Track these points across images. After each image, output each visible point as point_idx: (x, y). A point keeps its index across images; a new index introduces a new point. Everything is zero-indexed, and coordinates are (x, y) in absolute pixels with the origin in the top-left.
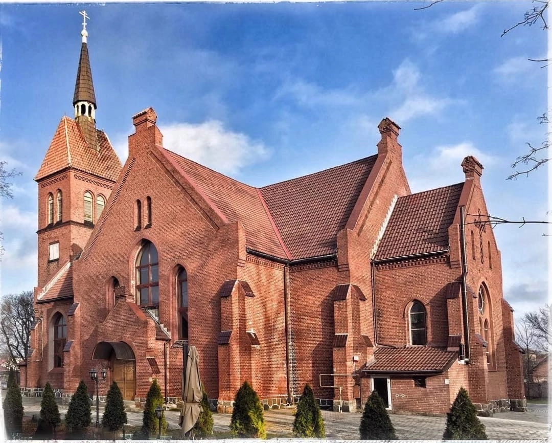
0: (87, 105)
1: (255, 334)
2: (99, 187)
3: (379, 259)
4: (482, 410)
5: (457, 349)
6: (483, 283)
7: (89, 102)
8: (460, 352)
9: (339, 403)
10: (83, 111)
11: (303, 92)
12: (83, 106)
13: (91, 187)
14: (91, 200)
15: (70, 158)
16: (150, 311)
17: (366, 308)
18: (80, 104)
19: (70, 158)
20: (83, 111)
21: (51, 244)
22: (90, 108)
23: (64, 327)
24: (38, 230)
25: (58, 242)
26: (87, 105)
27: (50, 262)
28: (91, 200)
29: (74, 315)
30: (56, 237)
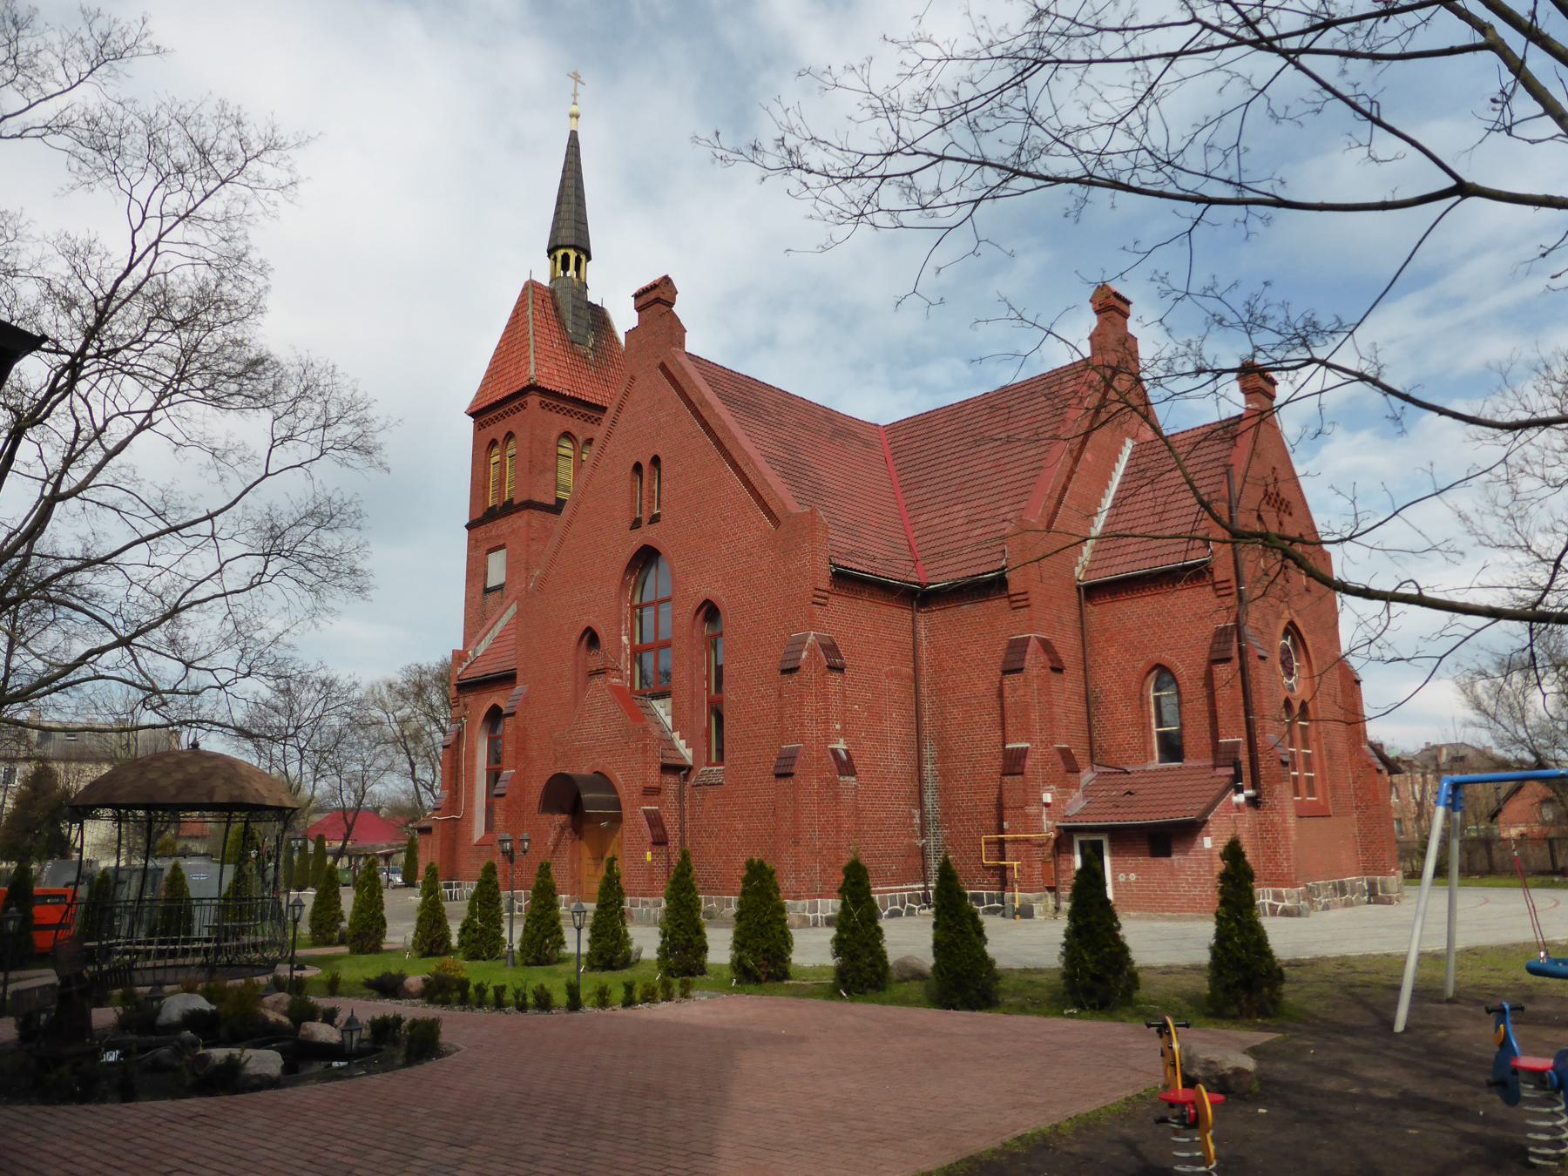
0: (572, 254)
1: (847, 752)
2: (588, 425)
3: (1096, 578)
4: (1287, 904)
5: (1231, 771)
6: (1292, 623)
7: (575, 248)
8: (1237, 777)
9: (1013, 899)
10: (565, 267)
11: (403, 797)
12: (566, 258)
13: (573, 424)
14: (571, 453)
15: (532, 367)
16: (654, 703)
17: (1067, 690)
18: (560, 253)
19: (532, 367)
20: (565, 267)
21: (491, 551)
22: (578, 260)
23: (662, 652)
24: (467, 521)
25: (502, 547)
26: (572, 254)
27: (487, 591)
28: (571, 453)
29: (1098, 312)
30: (498, 537)
